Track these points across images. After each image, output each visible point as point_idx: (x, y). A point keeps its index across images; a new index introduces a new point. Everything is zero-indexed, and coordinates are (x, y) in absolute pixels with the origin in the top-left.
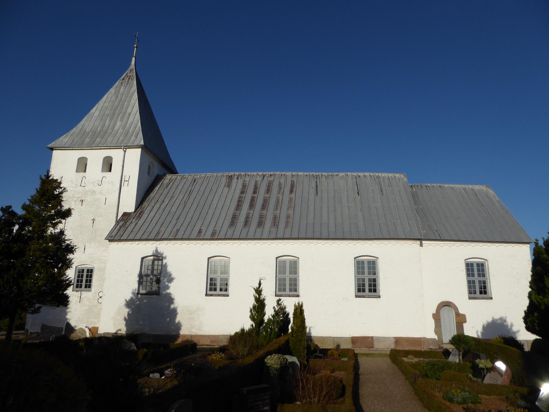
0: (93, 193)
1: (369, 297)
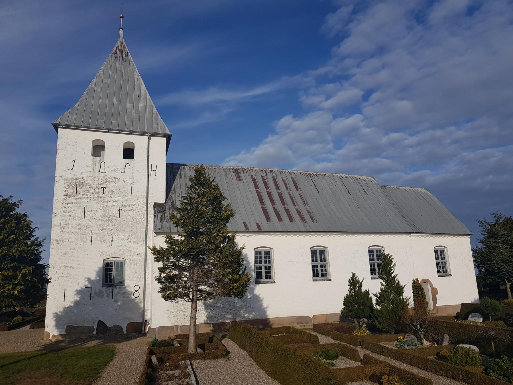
0: (116, 181)
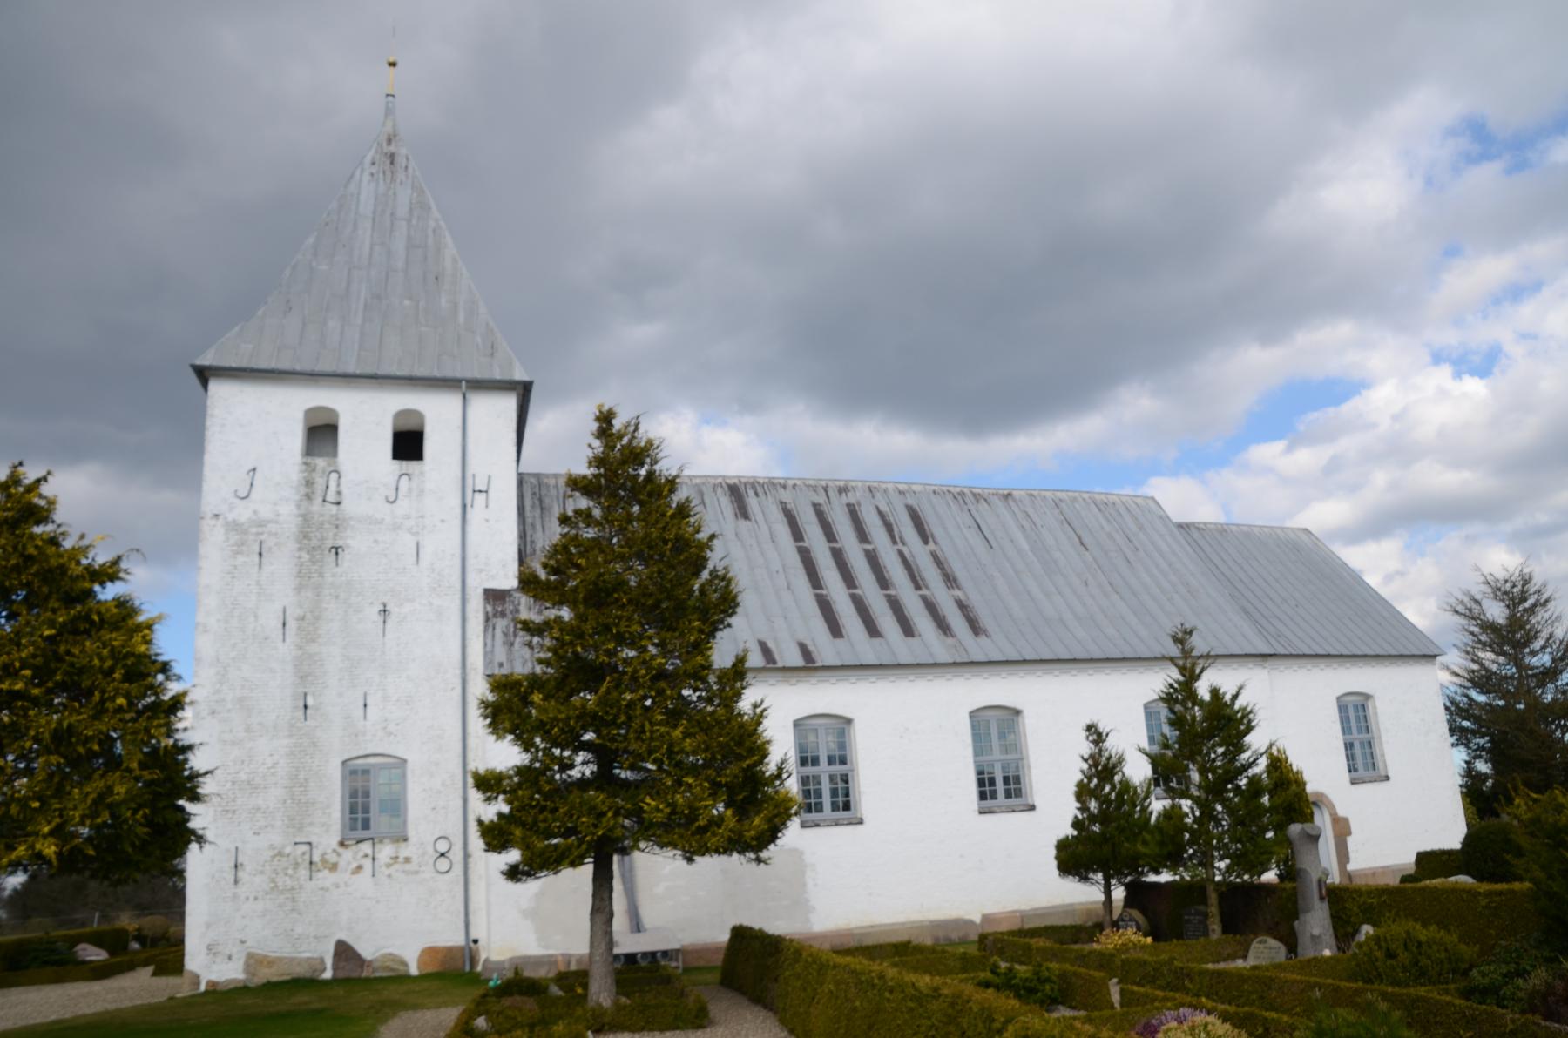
1: (837, 823)
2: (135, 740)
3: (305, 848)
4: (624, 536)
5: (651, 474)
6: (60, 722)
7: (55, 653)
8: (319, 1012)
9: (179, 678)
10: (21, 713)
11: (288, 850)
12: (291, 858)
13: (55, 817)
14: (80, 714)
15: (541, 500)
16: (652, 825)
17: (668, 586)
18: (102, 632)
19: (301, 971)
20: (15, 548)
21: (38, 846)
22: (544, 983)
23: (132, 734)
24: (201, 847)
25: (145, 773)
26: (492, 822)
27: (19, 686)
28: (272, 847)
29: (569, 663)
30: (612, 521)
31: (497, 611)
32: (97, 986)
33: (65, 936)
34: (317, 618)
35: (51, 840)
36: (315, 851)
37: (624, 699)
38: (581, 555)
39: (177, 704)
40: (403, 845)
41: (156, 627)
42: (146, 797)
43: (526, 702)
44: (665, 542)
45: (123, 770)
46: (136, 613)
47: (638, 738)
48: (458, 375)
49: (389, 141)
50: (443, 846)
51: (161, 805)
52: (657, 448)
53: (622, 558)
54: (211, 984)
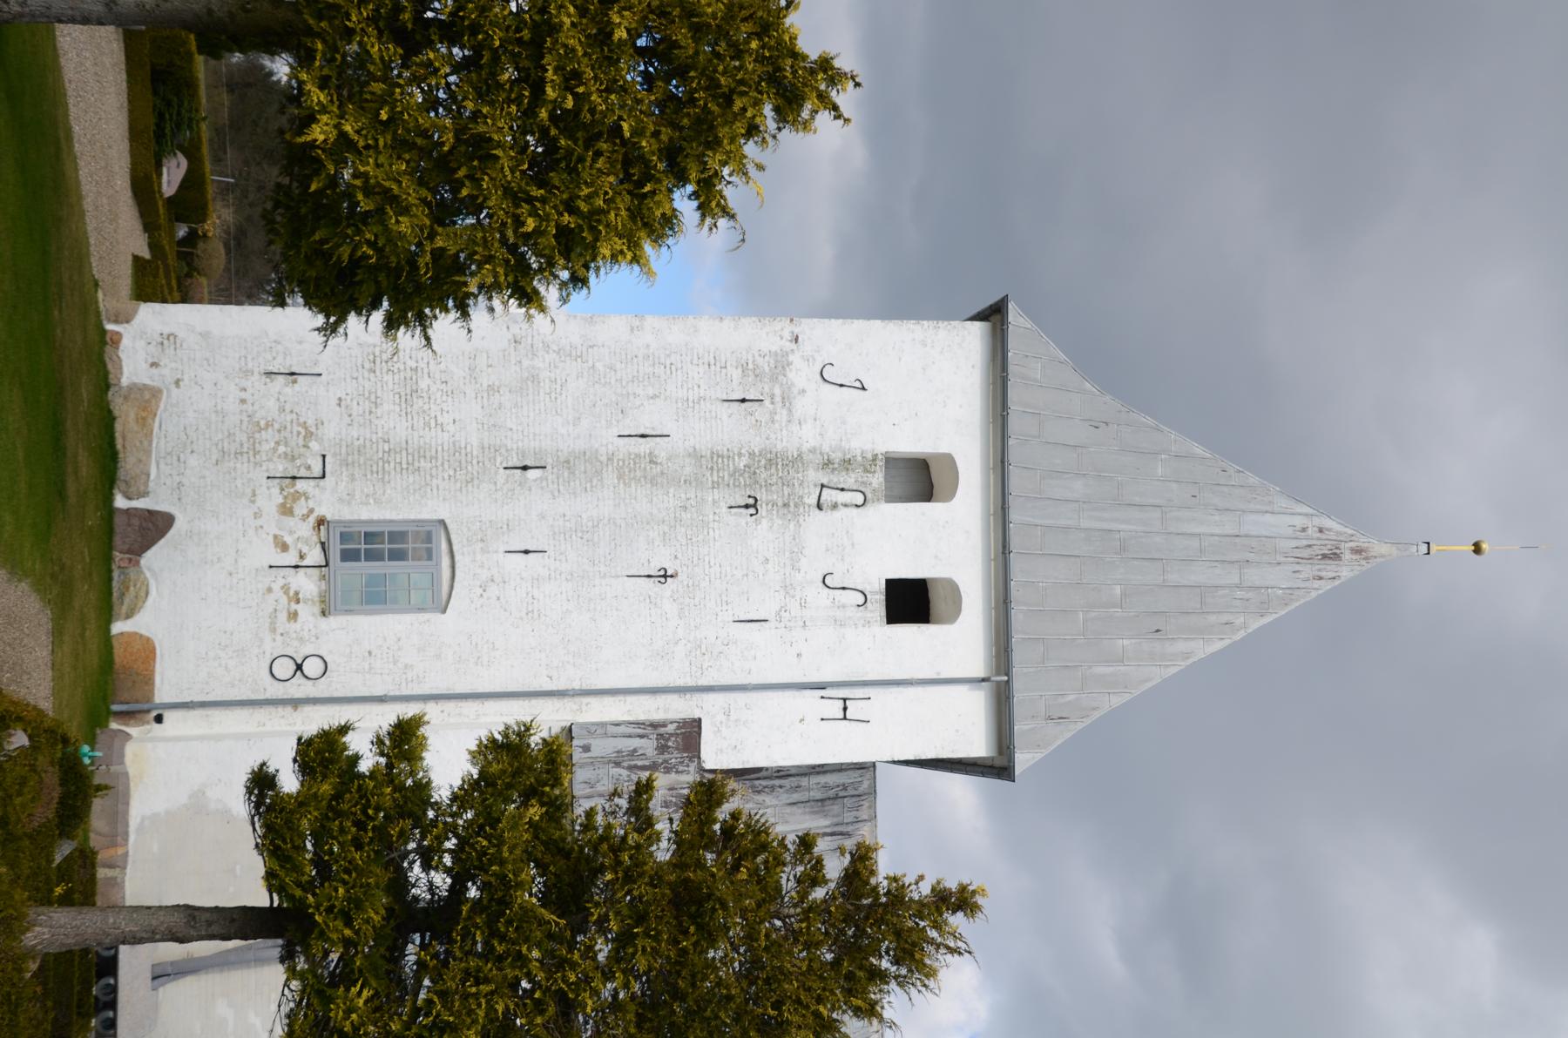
2: (475, 243)
3: (317, 471)
4: (786, 938)
5: (880, 976)
6: (500, 145)
7: (599, 136)
8: (61, 494)
9: (564, 300)
10: (513, 96)
11: (314, 445)
12: (302, 450)
13: (366, 140)
14: (512, 172)
15: (837, 797)
16: (327, 1000)
17: (708, 1013)
18: (627, 198)
19: (128, 463)
20: (742, 82)
21: (325, 118)
22: (80, 832)
23: (484, 238)
24: (318, 329)
25: (428, 257)
26: (346, 748)
27: (551, 93)
28: (320, 423)
29: (588, 859)
30: (807, 919)
31: (668, 740)
32: (122, 182)
33: (200, 138)
34: (653, 482)
35: (333, 136)
36: (312, 482)
37: (529, 950)
38: (754, 872)
39: (528, 297)
40: (317, 609)
41: (636, 268)
42: (393, 259)
43: (529, 794)
44: (777, 1005)
45: (431, 227)
46: (655, 241)
47: (467, 973)
48: (1016, 671)
49: (1357, 551)
50: (311, 667)
51: (382, 277)
52: (925, 986)
53: (751, 937)
54: (116, 340)
